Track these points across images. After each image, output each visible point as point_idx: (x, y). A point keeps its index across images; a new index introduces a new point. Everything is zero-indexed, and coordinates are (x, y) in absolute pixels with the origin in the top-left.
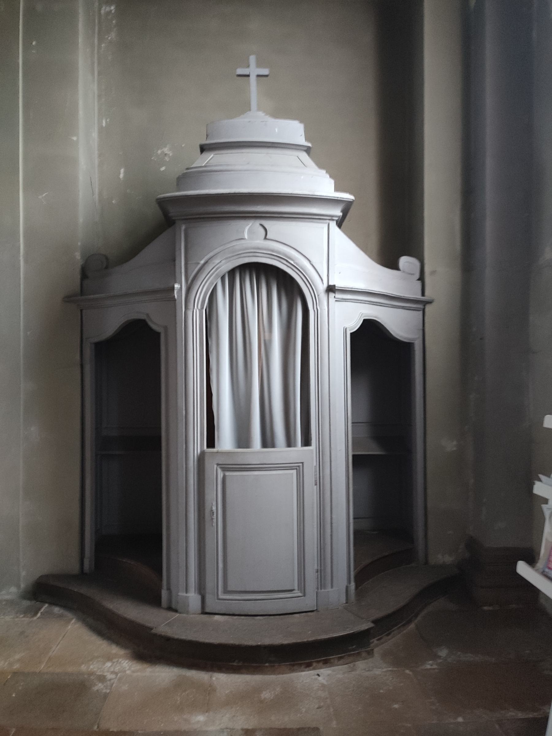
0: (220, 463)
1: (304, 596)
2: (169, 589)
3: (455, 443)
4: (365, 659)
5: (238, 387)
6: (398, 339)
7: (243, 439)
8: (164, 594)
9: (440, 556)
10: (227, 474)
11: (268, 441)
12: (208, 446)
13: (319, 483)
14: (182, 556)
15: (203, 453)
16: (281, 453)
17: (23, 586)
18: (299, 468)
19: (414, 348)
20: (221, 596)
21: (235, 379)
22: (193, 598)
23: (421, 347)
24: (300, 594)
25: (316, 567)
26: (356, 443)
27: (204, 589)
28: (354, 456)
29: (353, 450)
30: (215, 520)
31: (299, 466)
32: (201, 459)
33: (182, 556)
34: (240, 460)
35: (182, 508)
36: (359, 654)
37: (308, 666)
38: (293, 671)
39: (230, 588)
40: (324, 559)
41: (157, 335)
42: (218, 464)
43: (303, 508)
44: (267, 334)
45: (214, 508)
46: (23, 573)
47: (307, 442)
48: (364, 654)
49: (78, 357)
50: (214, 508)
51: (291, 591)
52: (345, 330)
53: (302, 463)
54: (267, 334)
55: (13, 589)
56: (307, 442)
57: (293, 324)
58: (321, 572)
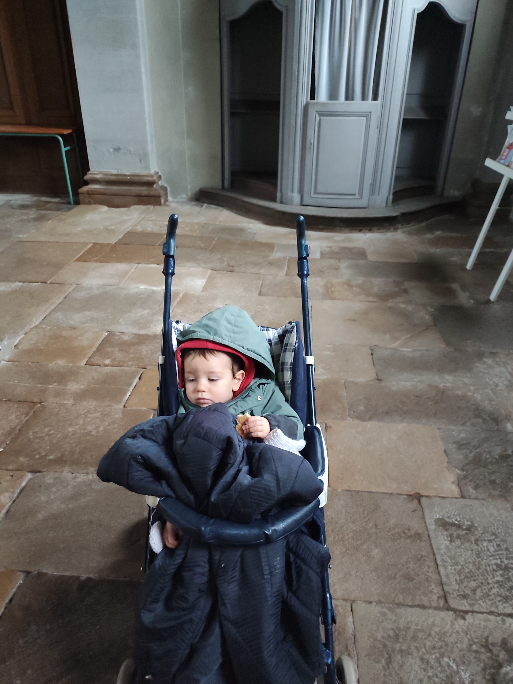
0: (318, 110)
1: (361, 198)
2: (281, 192)
3: (481, 109)
4: (392, 232)
5: (333, 56)
6: (451, 18)
7: (333, 95)
8: (279, 195)
9: (452, 191)
10: (322, 118)
11: (349, 96)
12: (311, 99)
13: (380, 128)
14: (291, 172)
15: (307, 104)
16: (358, 104)
17: (189, 194)
18: (367, 115)
19: (465, 28)
20: (313, 195)
21: (331, 48)
22: (296, 197)
23: (471, 29)
24: (359, 197)
25: (370, 182)
26: (407, 110)
27: (303, 191)
28: (404, 119)
29: (404, 115)
30: (312, 149)
31: (368, 115)
32: (306, 108)
33: (291, 172)
34: (331, 109)
35: (292, 141)
36: (389, 229)
37: (360, 231)
38: (351, 232)
39: (318, 191)
40: (378, 165)
41: (280, 13)
42: (316, 111)
43: (401, 18)
44: (357, 13)
45: (312, 141)
46: (189, 187)
47: (375, 97)
48: (392, 229)
49: (217, 33)
50: (312, 141)
51: (354, 195)
52: (414, 11)
53: (371, 112)
54: (357, 13)
55: (184, 196)
56: (375, 97)
57: (376, 7)
58: (373, 186)
